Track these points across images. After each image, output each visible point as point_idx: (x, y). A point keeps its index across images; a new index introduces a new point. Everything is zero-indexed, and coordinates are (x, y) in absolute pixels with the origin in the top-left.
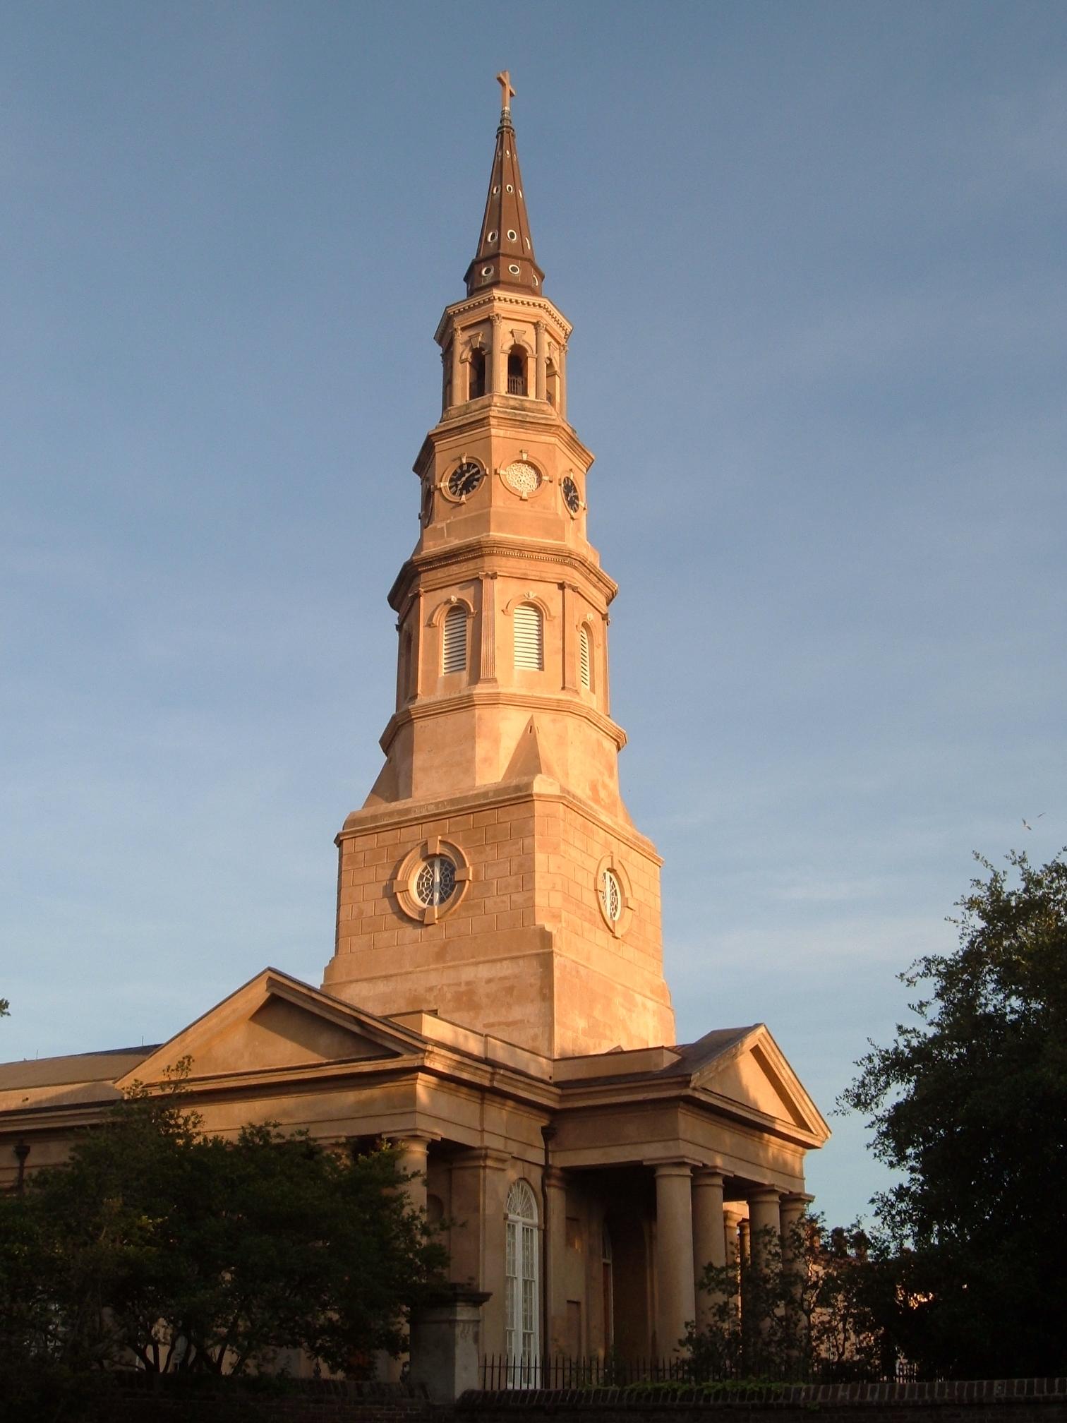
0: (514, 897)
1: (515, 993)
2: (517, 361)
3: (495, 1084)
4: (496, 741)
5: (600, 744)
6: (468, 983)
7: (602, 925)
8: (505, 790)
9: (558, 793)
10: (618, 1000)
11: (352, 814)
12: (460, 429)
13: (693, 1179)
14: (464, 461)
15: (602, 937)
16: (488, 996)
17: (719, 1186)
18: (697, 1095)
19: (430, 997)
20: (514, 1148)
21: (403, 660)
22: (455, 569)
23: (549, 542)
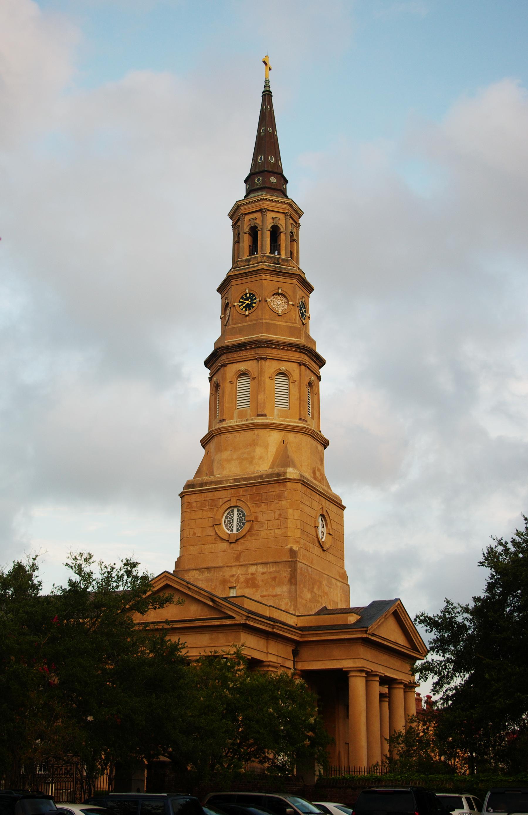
0: (276, 531)
1: (277, 580)
2: (275, 232)
3: (275, 630)
4: (266, 447)
5: (317, 448)
6: (252, 574)
7: (317, 544)
8: (270, 475)
9: (299, 478)
10: (325, 582)
11: (188, 481)
12: (246, 274)
13: (404, 689)
14: (247, 291)
15: (317, 550)
16: (263, 581)
17: (402, 688)
18: (370, 637)
19: (233, 580)
20: (280, 661)
21: (213, 397)
22: (244, 353)
23: (293, 340)
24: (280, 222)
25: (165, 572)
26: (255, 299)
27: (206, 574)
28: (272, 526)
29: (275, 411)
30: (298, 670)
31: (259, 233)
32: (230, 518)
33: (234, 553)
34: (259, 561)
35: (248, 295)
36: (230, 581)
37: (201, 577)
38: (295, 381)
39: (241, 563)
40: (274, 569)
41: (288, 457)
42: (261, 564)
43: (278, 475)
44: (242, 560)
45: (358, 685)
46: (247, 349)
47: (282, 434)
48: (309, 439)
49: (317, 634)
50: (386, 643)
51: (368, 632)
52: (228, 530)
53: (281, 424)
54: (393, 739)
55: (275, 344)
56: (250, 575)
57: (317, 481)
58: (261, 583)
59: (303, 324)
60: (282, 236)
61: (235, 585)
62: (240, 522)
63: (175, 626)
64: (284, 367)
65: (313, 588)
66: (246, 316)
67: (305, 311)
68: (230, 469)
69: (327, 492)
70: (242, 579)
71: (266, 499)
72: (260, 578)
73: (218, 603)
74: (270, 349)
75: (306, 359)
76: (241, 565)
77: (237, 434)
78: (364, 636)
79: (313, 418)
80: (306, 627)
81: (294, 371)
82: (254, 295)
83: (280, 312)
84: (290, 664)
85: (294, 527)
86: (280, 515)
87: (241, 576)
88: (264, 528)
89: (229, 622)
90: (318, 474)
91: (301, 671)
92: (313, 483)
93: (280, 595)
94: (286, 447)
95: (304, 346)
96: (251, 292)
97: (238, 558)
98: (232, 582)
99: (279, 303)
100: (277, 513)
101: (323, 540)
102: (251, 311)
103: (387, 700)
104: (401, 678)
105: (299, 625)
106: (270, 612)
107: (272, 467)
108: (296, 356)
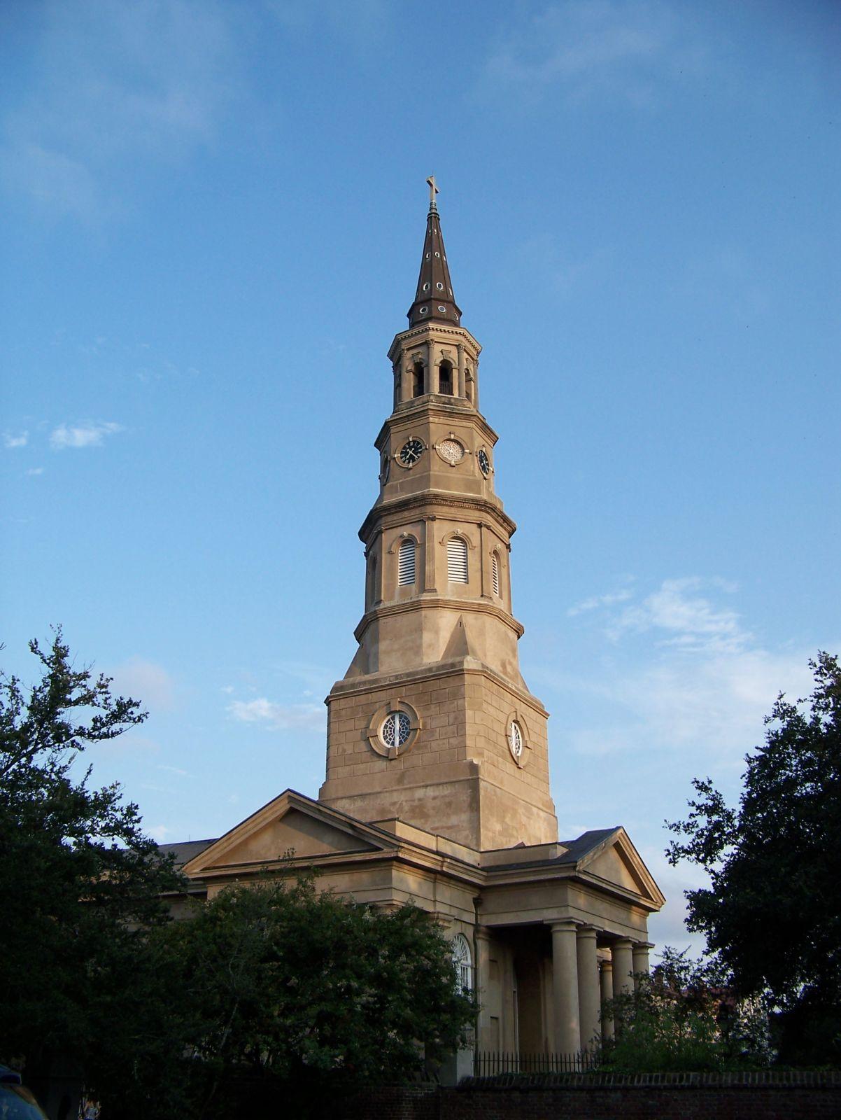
0: (451, 740)
3: (444, 869)
4: (437, 632)
5: (507, 635)
6: (420, 800)
7: (510, 759)
8: (443, 667)
9: (481, 669)
10: (521, 811)
11: (336, 683)
14: (411, 439)
15: (511, 767)
16: (434, 808)
20: (454, 912)
22: (406, 514)
24: (451, 355)
25: (289, 790)
26: (421, 447)
27: (359, 803)
28: (446, 734)
29: (449, 585)
30: (483, 926)
31: (425, 369)
32: (390, 728)
33: (396, 774)
34: (429, 783)
35: (412, 444)
36: (390, 810)
37: (352, 806)
38: (475, 547)
39: (405, 787)
40: (449, 791)
41: (466, 643)
42: (431, 785)
43: (453, 665)
44: (405, 782)
45: (566, 943)
46: (410, 509)
47: (459, 614)
48: (496, 622)
49: (507, 875)
50: (604, 886)
51: (577, 869)
52: (388, 743)
53: (456, 601)
54: (609, 1009)
55: (446, 500)
56: (416, 802)
57: (508, 677)
58: (431, 812)
59: (485, 479)
60: (455, 373)
61: (397, 816)
62: (404, 732)
63: (297, 865)
64: (460, 529)
65: (504, 817)
66: (411, 469)
67: (488, 464)
68: (391, 664)
69: (524, 693)
70: (406, 808)
71: (437, 699)
72: (430, 804)
73: (358, 830)
74: (440, 507)
75: (489, 519)
76: (406, 789)
77: (399, 618)
78: (572, 874)
79: (501, 597)
80: (493, 866)
81: (473, 534)
82: (419, 443)
83: (453, 463)
84: (470, 918)
85: (475, 733)
86: (456, 718)
87: (404, 803)
88: (434, 738)
89: (374, 856)
90: (509, 669)
91: (488, 927)
92: (502, 678)
93: (458, 825)
94: (464, 630)
95: (485, 502)
96: (415, 439)
97: (400, 780)
98: (393, 812)
99: (451, 451)
100: (452, 715)
101: (519, 754)
102: (415, 463)
103: (611, 968)
104: (627, 935)
105: (482, 865)
106: (437, 844)
107: (446, 654)
108: (475, 515)
